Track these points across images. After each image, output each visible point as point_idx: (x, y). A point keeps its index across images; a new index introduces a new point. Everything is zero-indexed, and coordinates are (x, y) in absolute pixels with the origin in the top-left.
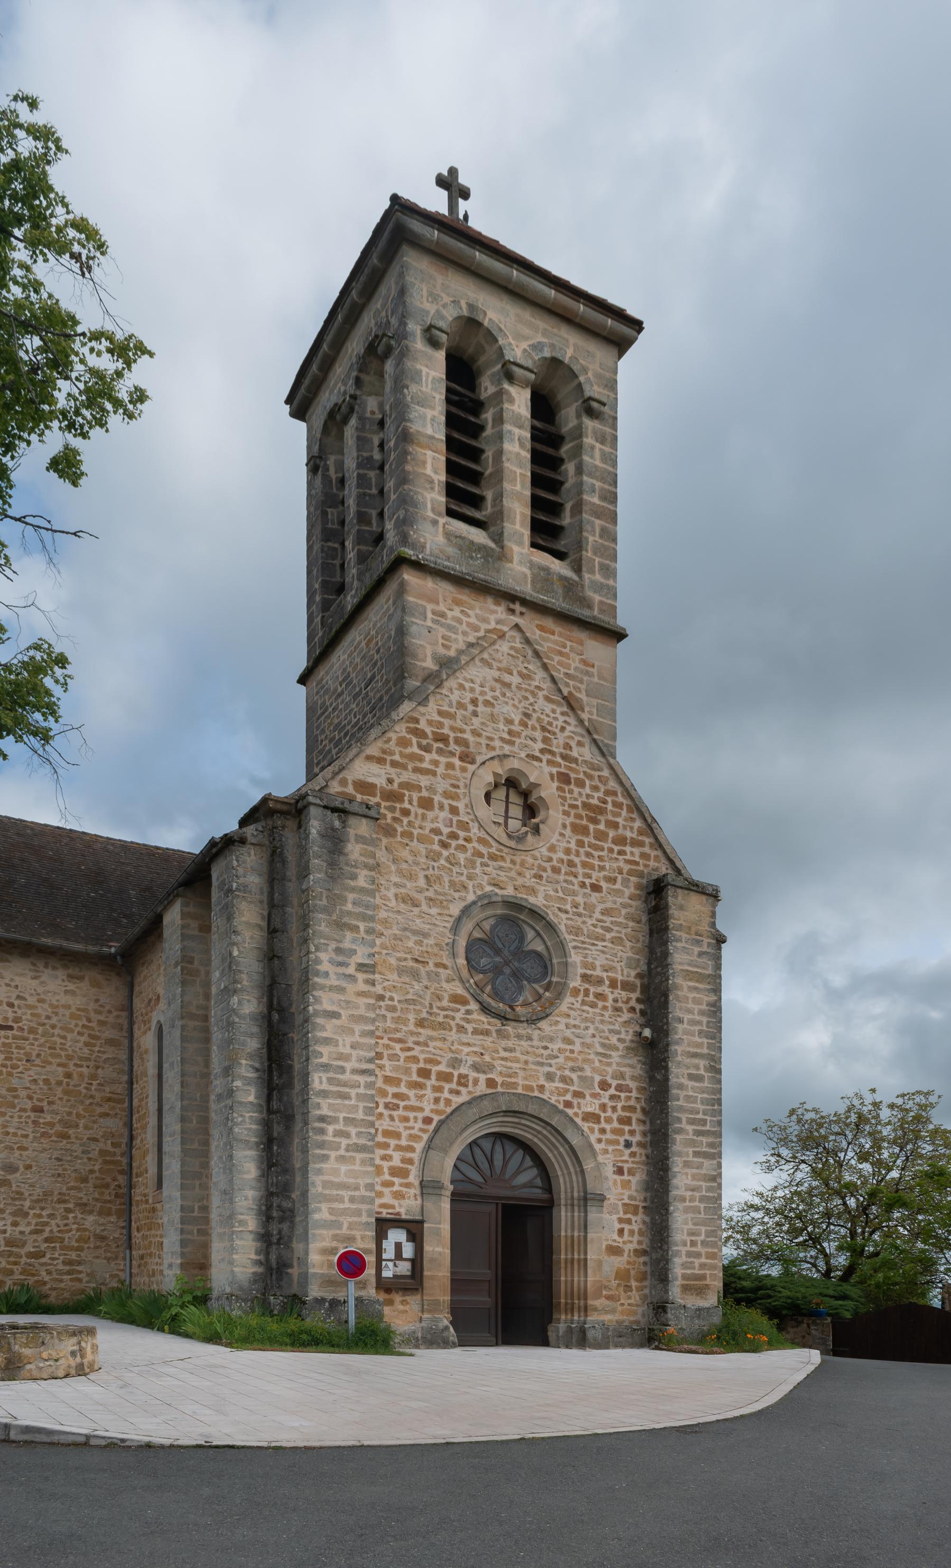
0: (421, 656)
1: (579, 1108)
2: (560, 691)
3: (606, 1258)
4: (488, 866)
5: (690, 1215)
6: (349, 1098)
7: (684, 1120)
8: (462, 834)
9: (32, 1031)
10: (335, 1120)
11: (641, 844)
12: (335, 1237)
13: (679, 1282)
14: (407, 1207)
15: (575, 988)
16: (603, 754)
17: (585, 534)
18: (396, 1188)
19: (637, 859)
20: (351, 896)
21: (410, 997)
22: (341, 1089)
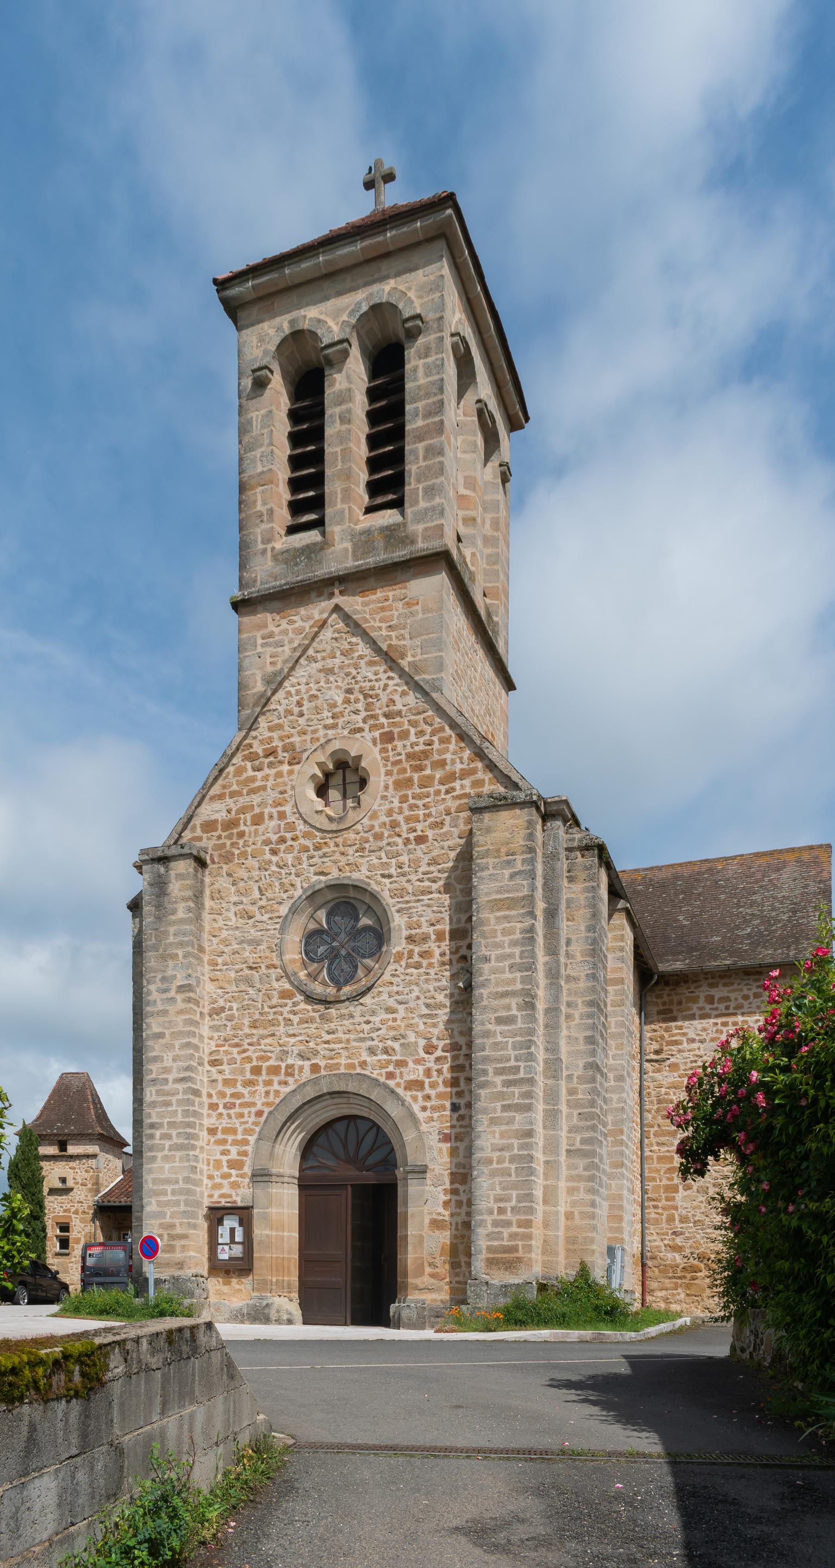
0: (252, 684)
5: (497, 1179)
8: (289, 835)
10: (161, 1125)
13: (484, 1255)
15: (398, 952)
16: (426, 694)
18: (233, 1179)
20: (172, 930)
21: (246, 1002)
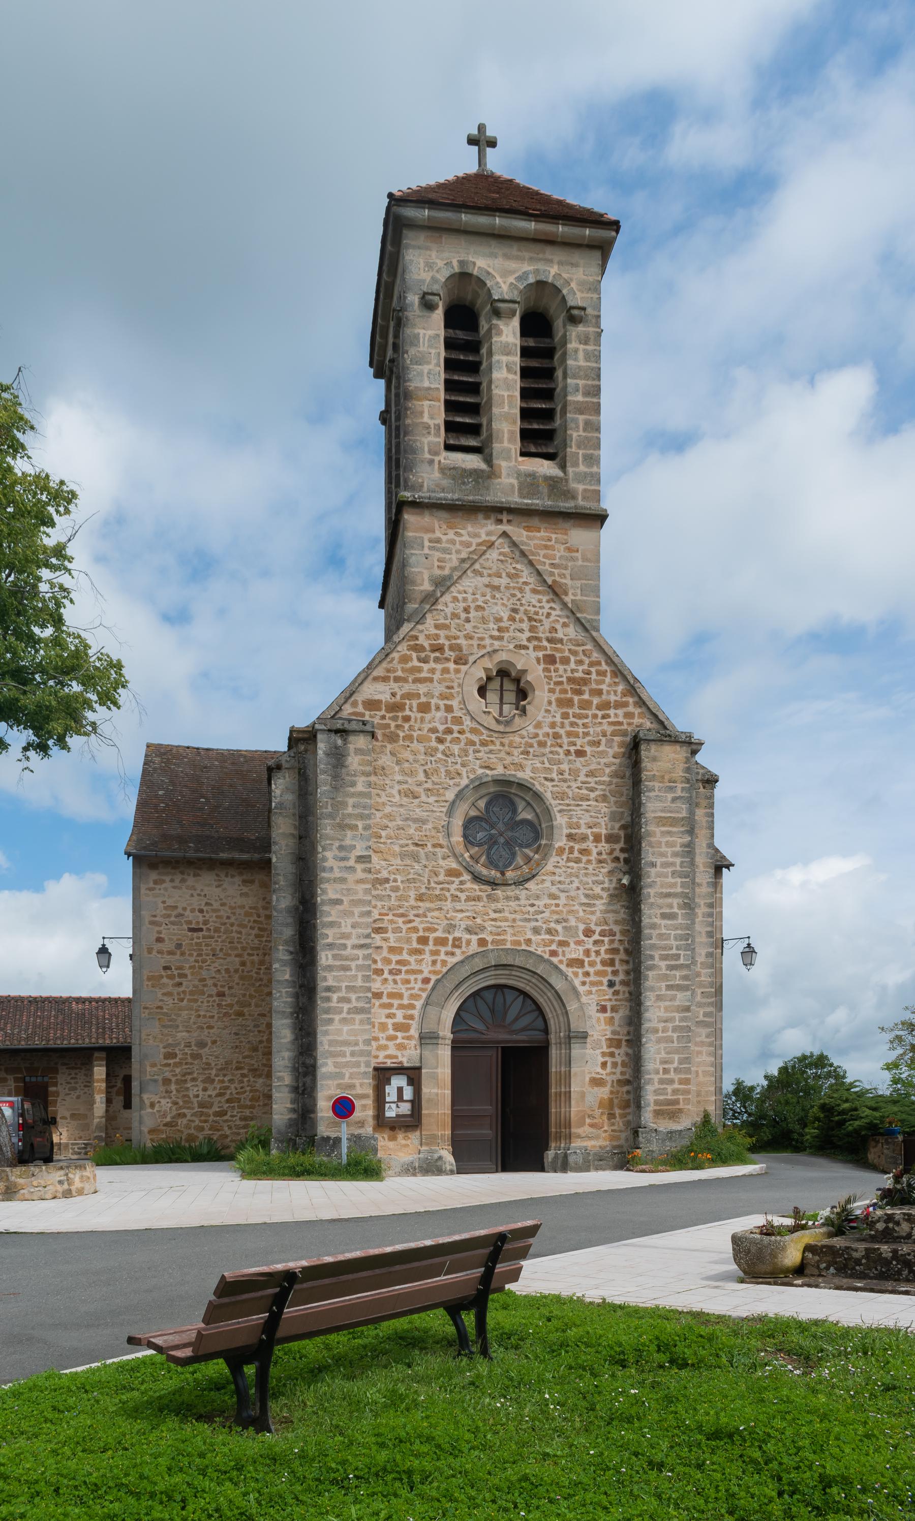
0: (419, 581)
1: (564, 955)
2: (545, 581)
3: (590, 1089)
4: (479, 751)
5: (663, 1045)
6: (350, 969)
7: (657, 957)
8: (456, 728)
9: (217, 930)
10: (338, 989)
11: (625, 705)
12: (339, 1086)
13: (652, 1108)
14: (408, 1057)
15: (560, 847)
16: (586, 630)
17: (569, 432)
18: (399, 1041)
19: (621, 719)
20: (351, 801)
21: (411, 876)
22: (344, 963)
